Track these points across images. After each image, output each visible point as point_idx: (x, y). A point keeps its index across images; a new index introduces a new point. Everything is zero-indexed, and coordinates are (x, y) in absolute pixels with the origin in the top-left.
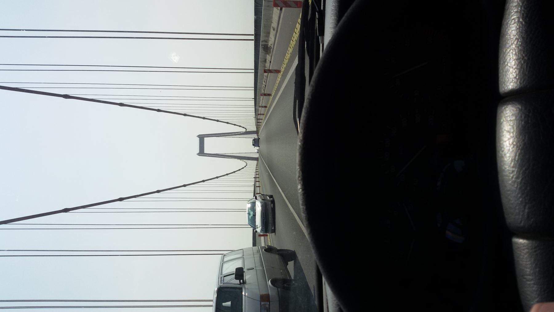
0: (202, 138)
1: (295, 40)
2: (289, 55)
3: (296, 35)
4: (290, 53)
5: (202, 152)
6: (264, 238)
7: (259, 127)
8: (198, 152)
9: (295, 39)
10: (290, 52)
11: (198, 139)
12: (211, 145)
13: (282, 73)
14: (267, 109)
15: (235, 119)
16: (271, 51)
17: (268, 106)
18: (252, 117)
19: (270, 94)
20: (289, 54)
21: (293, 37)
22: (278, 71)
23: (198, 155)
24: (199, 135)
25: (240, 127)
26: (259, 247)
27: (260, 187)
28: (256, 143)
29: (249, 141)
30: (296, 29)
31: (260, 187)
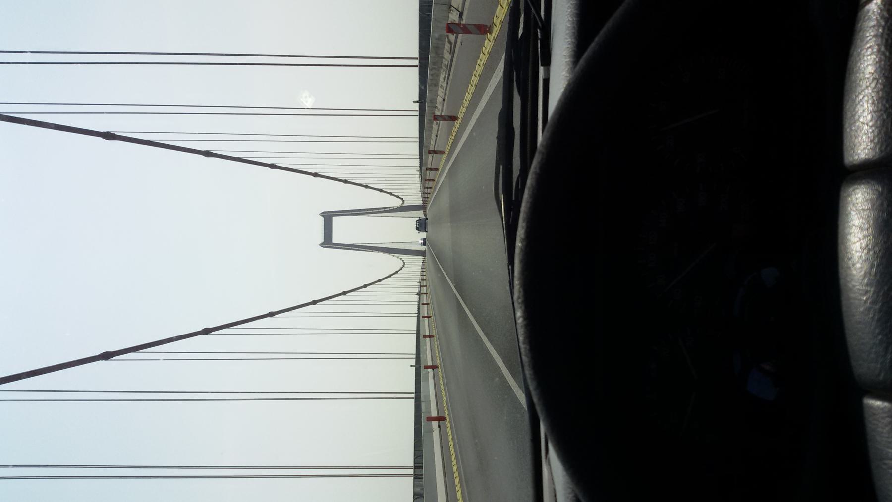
0: (328, 217)
1: (494, 37)
3: (476, 78)
5: (328, 242)
8: (322, 240)
12: (342, 230)
22: (442, 152)
23: (322, 246)
24: (324, 212)
28: (422, 225)
29: (409, 222)
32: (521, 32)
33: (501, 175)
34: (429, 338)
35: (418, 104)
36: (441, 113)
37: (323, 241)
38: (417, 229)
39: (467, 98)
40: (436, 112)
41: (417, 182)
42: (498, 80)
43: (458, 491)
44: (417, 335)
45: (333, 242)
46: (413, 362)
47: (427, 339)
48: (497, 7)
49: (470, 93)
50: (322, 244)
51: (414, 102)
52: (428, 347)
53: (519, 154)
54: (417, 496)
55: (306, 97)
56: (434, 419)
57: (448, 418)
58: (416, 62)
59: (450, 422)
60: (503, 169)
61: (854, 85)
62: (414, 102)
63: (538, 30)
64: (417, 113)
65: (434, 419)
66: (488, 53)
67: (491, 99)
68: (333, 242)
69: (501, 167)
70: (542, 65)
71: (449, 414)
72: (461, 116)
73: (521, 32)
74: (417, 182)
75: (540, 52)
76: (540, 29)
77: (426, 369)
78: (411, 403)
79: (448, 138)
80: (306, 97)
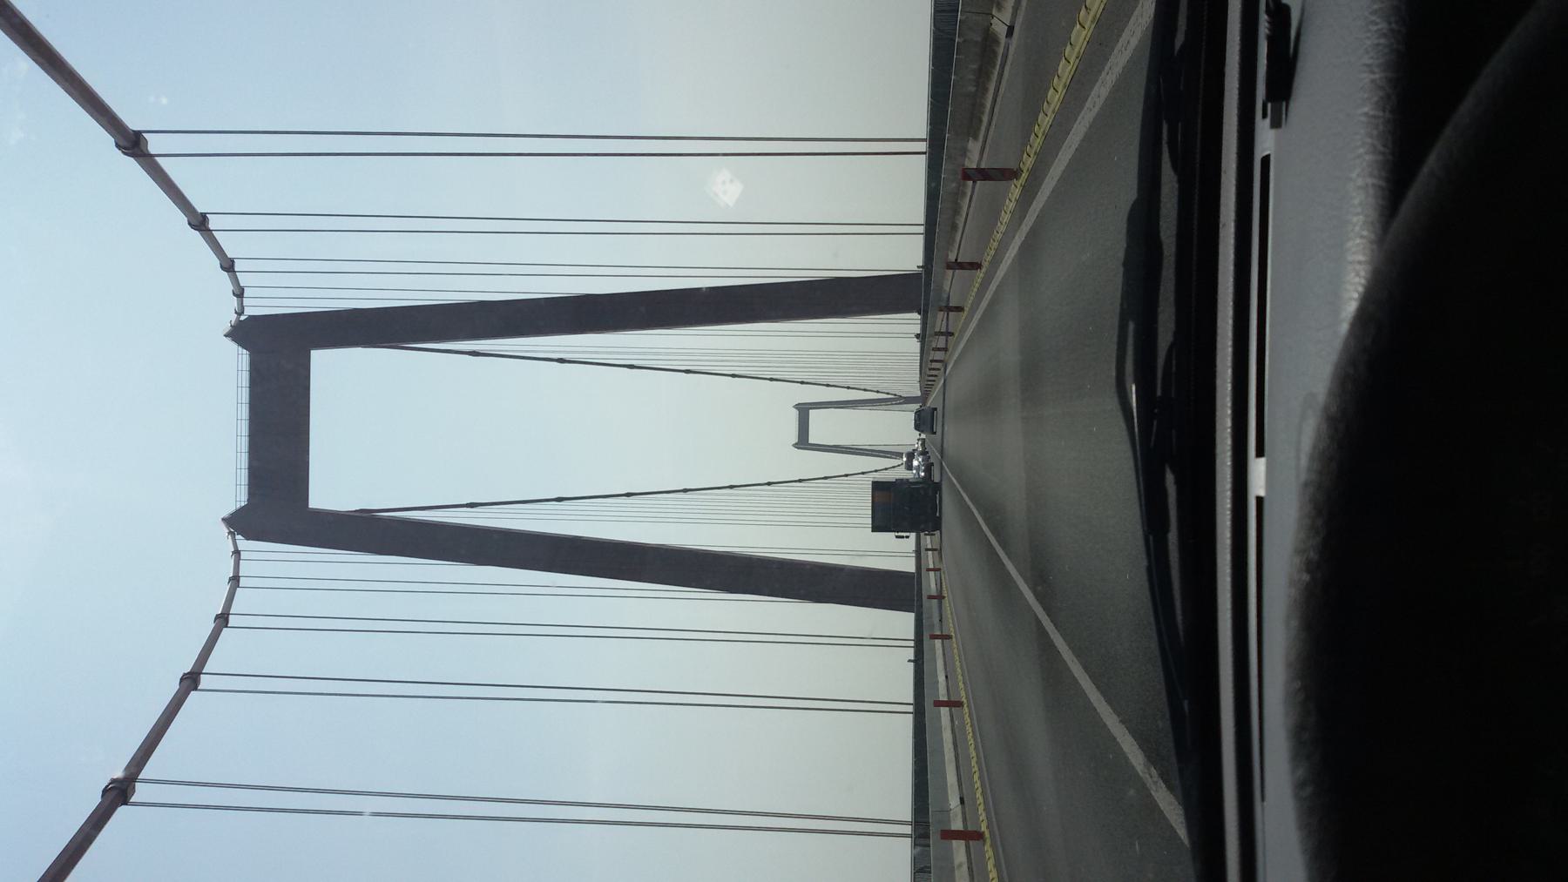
0: (804, 410)
1: (1044, 131)
2: (1038, 140)
3: (1084, 33)
4: (1035, 153)
5: (803, 442)
6: (943, 643)
7: (934, 381)
8: (795, 440)
9: (1052, 106)
10: (1042, 130)
11: (795, 413)
12: (823, 427)
13: (1024, 175)
14: (980, 274)
15: (789, 359)
16: (988, 105)
17: (986, 261)
18: (258, 292)
19: (977, 263)
20: (1040, 135)
21: (1037, 126)
22: (1009, 174)
23: (798, 448)
24: (799, 404)
25: (174, 686)
26: (938, 515)
27: (952, 334)
28: (924, 421)
29: (906, 417)
30: (1046, 103)
31: (952, 334)
32: (1180, 40)
33: (1130, 341)
34: (962, 843)
36: (979, 163)
37: (797, 441)
38: (916, 429)
39: (1003, 219)
40: (966, 163)
42: (1134, 42)
43: (989, 859)
45: (310, 507)
46: (910, 654)
48: (1047, 90)
49: (1013, 200)
50: (796, 444)
51: (909, 661)
52: (939, 652)
54: (920, 868)
55: (724, 183)
56: (931, 570)
57: (987, 835)
58: (911, 709)
59: (993, 846)
60: (1137, 332)
62: (909, 661)
64: (921, 229)
65: (931, 570)
66: (1043, 134)
67: (1116, 89)
71: (955, 633)
72: (985, 265)
73: (1180, 40)
77: (946, 841)
78: (908, 722)
79: (1026, 141)
80: (724, 183)
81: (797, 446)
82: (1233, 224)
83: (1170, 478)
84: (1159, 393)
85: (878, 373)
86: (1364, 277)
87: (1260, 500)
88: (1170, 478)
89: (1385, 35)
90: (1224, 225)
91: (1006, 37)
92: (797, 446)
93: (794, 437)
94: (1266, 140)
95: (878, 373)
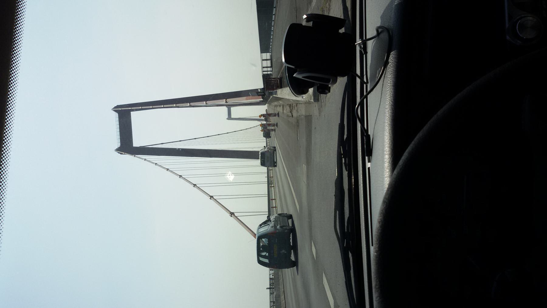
5: (230, 117)
23: (228, 120)
32: (345, 137)
33: (337, 215)
35: (269, 290)
41: (265, 195)
44: (268, 184)
46: (266, 175)
47: (274, 208)
50: (228, 118)
53: (347, 196)
60: (339, 213)
61: (394, 74)
63: (364, 137)
68: (232, 117)
69: (337, 212)
70: (367, 156)
73: (345, 137)
74: (265, 195)
75: (311, 80)
76: (365, 137)
78: (266, 143)
81: (227, 119)
82: (362, 184)
83: (350, 255)
84: (346, 231)
85: (258, 140)
86: (389, 177)
87: (369, 168)
88: (350, 255)
89: (396, 55)
90: (360, 185)
91: (293, 230)
92: (227, 119)
93: (227, 117)
94: (368, 165)
95: (258, 140)
